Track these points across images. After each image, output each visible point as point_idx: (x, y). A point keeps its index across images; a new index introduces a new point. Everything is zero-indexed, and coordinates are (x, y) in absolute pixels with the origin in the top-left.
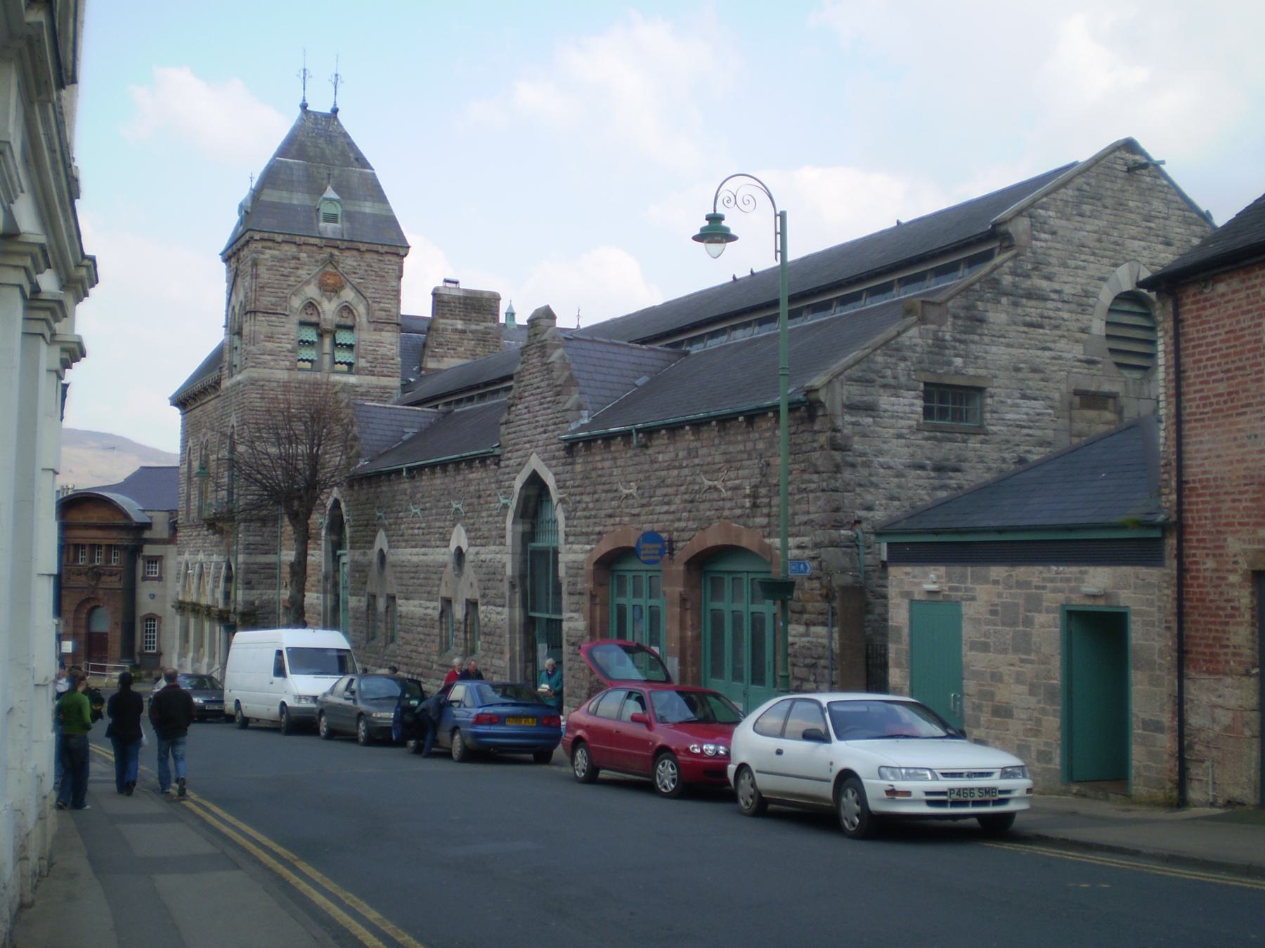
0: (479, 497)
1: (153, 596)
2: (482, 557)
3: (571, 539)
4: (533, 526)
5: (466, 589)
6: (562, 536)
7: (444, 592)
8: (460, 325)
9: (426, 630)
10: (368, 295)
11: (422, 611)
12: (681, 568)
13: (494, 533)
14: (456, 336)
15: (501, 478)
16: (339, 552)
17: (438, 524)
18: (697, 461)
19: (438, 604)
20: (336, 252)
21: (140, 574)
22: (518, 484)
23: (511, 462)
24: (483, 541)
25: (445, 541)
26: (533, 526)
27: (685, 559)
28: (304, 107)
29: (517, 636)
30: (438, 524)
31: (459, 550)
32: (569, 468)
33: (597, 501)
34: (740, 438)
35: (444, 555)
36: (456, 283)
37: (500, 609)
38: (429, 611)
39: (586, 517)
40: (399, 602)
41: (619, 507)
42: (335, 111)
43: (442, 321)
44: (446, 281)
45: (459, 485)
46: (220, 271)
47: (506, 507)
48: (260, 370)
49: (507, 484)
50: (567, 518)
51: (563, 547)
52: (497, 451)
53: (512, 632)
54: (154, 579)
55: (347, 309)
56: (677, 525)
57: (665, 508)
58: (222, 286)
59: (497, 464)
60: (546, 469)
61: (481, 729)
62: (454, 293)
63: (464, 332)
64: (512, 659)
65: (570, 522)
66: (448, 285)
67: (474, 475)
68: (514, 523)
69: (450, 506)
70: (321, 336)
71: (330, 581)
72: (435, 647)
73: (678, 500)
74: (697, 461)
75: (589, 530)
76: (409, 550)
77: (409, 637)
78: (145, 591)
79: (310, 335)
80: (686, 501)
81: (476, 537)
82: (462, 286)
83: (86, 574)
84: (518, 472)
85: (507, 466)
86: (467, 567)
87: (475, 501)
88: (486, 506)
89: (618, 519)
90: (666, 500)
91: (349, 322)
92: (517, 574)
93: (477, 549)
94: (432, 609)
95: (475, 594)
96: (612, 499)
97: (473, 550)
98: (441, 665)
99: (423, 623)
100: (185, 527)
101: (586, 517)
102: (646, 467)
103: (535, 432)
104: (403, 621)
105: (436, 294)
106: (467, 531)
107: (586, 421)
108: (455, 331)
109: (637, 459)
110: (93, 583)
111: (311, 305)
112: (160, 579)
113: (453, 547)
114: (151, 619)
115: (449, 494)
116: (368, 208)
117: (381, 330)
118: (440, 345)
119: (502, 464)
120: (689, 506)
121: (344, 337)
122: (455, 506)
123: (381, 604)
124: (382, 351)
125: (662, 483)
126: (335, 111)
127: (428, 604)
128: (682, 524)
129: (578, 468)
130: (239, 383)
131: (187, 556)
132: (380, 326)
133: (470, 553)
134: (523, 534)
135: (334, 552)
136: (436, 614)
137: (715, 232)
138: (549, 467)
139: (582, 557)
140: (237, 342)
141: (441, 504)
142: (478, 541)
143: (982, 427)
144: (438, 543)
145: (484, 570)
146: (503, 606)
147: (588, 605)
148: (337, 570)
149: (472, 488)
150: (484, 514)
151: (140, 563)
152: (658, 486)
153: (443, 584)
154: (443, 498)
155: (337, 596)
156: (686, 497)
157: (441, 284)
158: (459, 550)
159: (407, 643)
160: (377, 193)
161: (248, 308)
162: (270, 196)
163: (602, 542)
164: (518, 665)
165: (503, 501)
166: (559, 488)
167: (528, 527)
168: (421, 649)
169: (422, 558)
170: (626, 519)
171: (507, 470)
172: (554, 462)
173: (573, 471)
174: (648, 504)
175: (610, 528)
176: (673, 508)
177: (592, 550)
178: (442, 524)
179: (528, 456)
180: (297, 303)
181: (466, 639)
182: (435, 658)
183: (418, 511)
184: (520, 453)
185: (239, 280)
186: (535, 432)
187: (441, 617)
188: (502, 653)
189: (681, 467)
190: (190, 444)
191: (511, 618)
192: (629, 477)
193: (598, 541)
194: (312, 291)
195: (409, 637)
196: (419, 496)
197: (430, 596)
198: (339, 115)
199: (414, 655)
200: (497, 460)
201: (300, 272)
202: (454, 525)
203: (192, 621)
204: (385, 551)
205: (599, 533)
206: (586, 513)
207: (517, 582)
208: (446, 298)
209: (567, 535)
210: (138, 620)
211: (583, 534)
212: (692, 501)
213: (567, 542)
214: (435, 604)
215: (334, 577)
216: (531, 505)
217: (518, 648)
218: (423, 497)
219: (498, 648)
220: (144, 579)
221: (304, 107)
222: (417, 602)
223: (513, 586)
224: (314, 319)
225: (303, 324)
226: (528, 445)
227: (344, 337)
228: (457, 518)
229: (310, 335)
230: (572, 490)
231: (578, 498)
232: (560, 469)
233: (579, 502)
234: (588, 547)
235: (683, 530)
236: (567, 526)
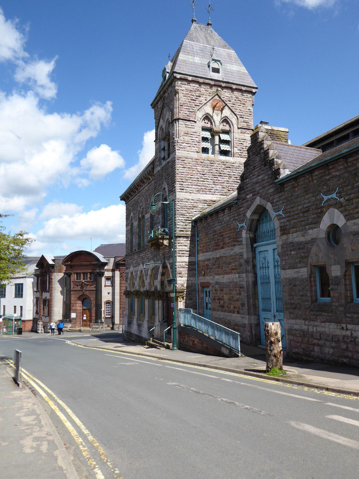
10: (237, 113)
16: (255, 245)
20: (220, 89)
55: (225, 120)
61: (97, 327)
70: (213, 136)
79: (207, 135)
91: (227, 128)
111: (207, 117)
117: (244, 133)
121: (224, 137)
131: (132, 269)
132: (244, 130)
135: (252, 247)
137: (109, 293)
143: (37, 330)
148: (254, 257)
155: (255, 274)
180: (200, 115)
190: (132, 214)
194: (208, 109)
201: (201, 98)
203: (136, 300)
215: (253, 261)
224: (209, 125)
225: (204, 129)
227: (224, 137)
229: (207, 135)
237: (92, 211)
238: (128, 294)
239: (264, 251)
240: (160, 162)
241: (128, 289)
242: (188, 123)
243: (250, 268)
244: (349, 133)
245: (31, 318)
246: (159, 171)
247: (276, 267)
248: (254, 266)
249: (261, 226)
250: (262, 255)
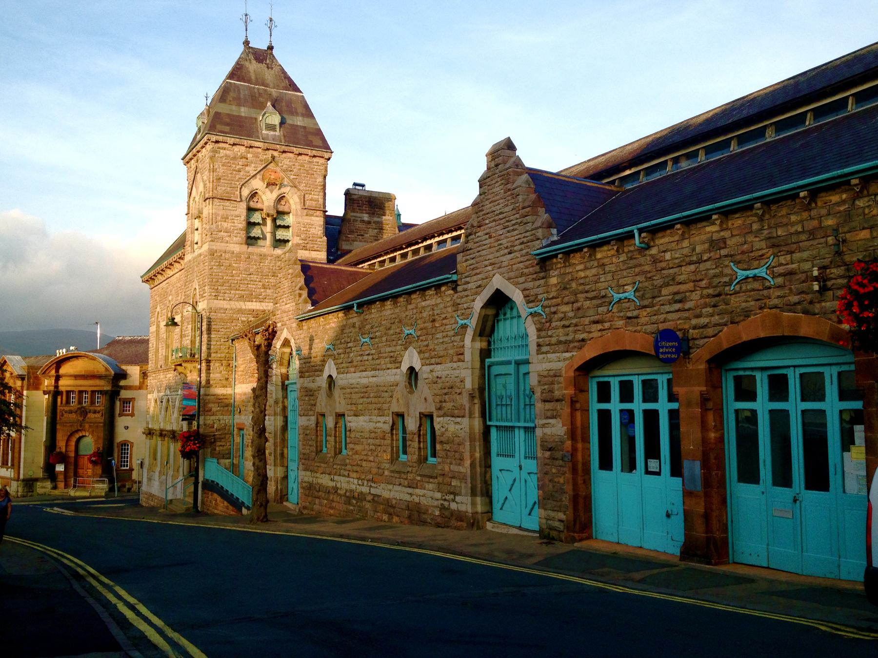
0: (434, 321)
1: (127, 428)
2: (439, 374)
3: (545, 349)
4: (489, 343)
5: (421, 401)
6: (533, 348)
7: (395, 408)
8: (366, 217)
9: (377, 442)
11: (371, 426)
12: (702, 366)
13: (451, 352)
14: (363, 226)
15: (458, 301)
17: (388, 349)
18: (723, 252)
19: (389, 419)
20: (276, 154)
21: (117, 411)
22: (479, 303)
23: (469, 286)
24: (438, 360)
25: (396, 362)
26: (489, 343)
27: (708, 357)
28: (246, 43)
29: (477, 444)
30: (388, 349)
31: (411, 369)
32: (542, 282)
33: (579, 309)
34: (793, 218)
35: (397, 375)
36: (363, 186)
37: (459, 420)
38: (380, 425)
39: (564, 326)
40: (348, 418)
41: (609, 311)
42: (271, 48)
43: (352, 214)
44: (355, 184)
45: (409, 313)
46: (182, 172)
47: (464, 327)
48: (218, 244)
49: (465, 306)
50: (539, 330)
51: (534, 358)
52: (455, 277)
53: (472, 439)
54: (128, 415)
56: (694, 322)
57: (677, 306)
58: (184, 186)
59: (455, 289)
60: (512, 287)
62: (361, 193)
63: (369, 223)
64: (472, 465)
65: (543, 334)
66: (357, 187)
67: (428, 303)
68: (473, 340)
69: (402, 332)
71: (280, 405)
72: (387, 456)
73: (695, 296)
74: (723, 252)
75: (570, 338)
76: (358, 374)
77: (358, 448)
78: (121, 422)
80: (708, 296)
81: (430, 357)
82: (367, 188)
83: (75, 412)
84: (477, 294)
85: (465, 290)
86: (337, 392)
87: (429, 325)
88: (442, 328)
89: (607, 325)
90: (677, 297)
92: (476, 386)
93: (432, 367)
94: (384, 423)
95: (431, 408)
96: (600, 305)
97: (427, 369)
98: (392, 472)
99: (373, 435)
100: (154, 372)
101: (564, 326)
102: (647, 268)
103: (498, 254)
104: (353, 435)
105: (348, 194)
106: (420, 353)
107: (555, 238)
108: (363, 221)
109: (632, 263)
110: (81, 419)
112: (132, 415)
113: (404, 367)
114: (124, 444)
115: (400, 321)
116: (299, 121)
117: (312, 215)
118: (352, 232)
119: (459, 288)
120: (714, 301)
122: (407, 332)
123: (330, 422)
124: (313, 231)
125: (673, 280)
126: (271, 48)
127: (379, 419)
128: (703, 321)
129: (554, 281)
130: (200, 255)
132: (311, 212)
133: (425, 372)
134: (481, 350)
136: (387, 428)
138: (516, 284)
139: (561, 365)
140: (197, 223)
141: (391, 332)
142: (433, 361)
144: (389, 366)
145: (440, 385)
146: (463, 417)
147: (567, 410)
148: (285, 397)
149: (425, 315)
150: (439, 336)
151: (118, 403)
152: (667, 285)
153: (394, 400)
154: (393, 326)
155: (286, 418)
156: (710, 291)
157: (351, 187)
158: (411, 369)
159: (357, 453)
160: (308, 113)
161: (207, 196)
162: (224, 108)
163: (585, 349)
164: (478, 469)
165: (461, 322)
166: (528, 302)
167: (484, 345)
168: (371, 458)
169: (371, 380)
170: (621, 323)
171: (466, 293)
172: (522, 279)
173: (547, 285)
174: (651, 306)
175: (596, 334)
176: (688, 305)
177: (571, 358)
178: (393, 349)
179: (489, 278)
181: (420, 448)
182: (387, 466)
183: (367, 340)
184: (480, 276)
185: (199, 176)
186: (498, 254)
187: (392, 430)
188: (462, 459)
189: (700, 261)
191: (471, 428)
192: (622, 282)
193: (580, 348)
195: (358, 448)
196: (367, 327)
197: (381, 412)
198: (274, 52)
199: (364, 464)
200: (454, 285)
201: (247, 168)
202: (406, 349)
204: (334, 375)
205: (583, 340)
206: (563, 323)
207: (477, 394)
208: (355, 197)
209: (539, 345)
210: (115, 445)
211: (560, 342)
212: (719, 295)
213: (539, 352)
214: (387, 418)
215: (283, 402)
216: (489, 324)
217: (477, 455)
218: (372, 328)
219: (457, 455)
220: (120, 415)
221: (246, 43)
222: (367, 418)
223: (472, 397)
226: (490, 268)
228: (408, 342)
230: (546, 303)
231: (553, 309)
232: (530, 285)
233: (555, 313)
234: (568, 355)
235: (705, 326)
236: (539, 337)
237: (484, 168)
238: (150, 434)
239: (505, 374)
240: (193, 248)
241: (150, 426)
242: (227, 203)
243: (279, 410)
244: (666, 161)
245: (537, 528)
246: (190, 261)
247: (528, 407)
248: (285, 408)
249: (501, 324)
250: (500, 380)
